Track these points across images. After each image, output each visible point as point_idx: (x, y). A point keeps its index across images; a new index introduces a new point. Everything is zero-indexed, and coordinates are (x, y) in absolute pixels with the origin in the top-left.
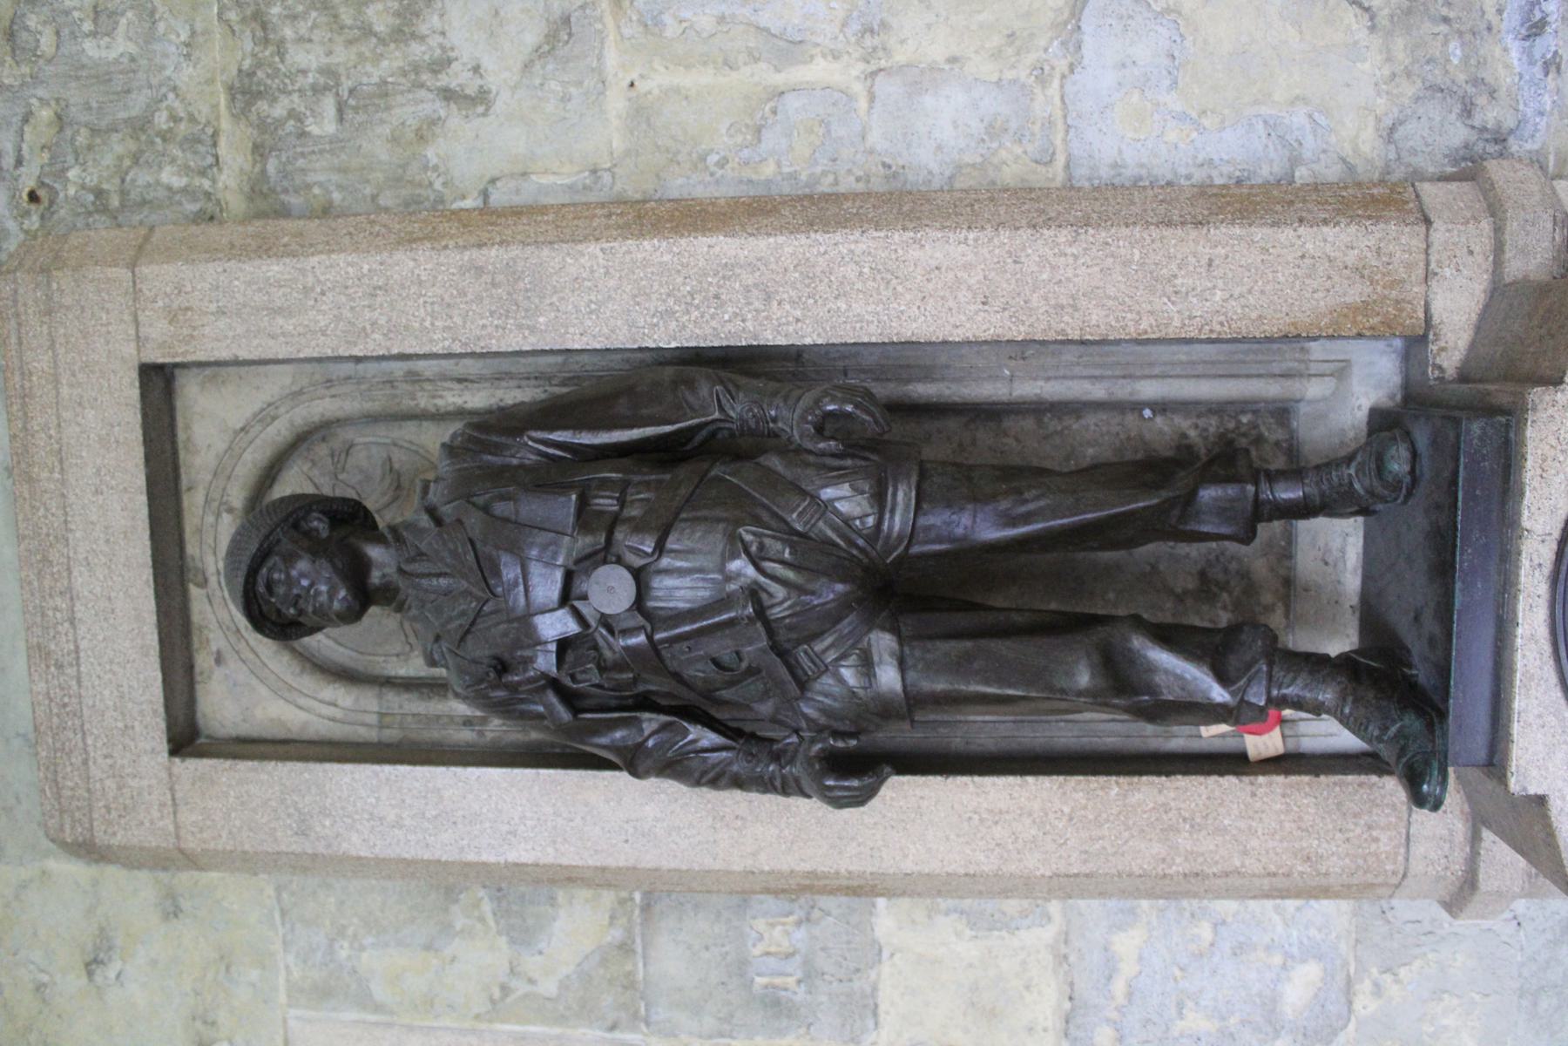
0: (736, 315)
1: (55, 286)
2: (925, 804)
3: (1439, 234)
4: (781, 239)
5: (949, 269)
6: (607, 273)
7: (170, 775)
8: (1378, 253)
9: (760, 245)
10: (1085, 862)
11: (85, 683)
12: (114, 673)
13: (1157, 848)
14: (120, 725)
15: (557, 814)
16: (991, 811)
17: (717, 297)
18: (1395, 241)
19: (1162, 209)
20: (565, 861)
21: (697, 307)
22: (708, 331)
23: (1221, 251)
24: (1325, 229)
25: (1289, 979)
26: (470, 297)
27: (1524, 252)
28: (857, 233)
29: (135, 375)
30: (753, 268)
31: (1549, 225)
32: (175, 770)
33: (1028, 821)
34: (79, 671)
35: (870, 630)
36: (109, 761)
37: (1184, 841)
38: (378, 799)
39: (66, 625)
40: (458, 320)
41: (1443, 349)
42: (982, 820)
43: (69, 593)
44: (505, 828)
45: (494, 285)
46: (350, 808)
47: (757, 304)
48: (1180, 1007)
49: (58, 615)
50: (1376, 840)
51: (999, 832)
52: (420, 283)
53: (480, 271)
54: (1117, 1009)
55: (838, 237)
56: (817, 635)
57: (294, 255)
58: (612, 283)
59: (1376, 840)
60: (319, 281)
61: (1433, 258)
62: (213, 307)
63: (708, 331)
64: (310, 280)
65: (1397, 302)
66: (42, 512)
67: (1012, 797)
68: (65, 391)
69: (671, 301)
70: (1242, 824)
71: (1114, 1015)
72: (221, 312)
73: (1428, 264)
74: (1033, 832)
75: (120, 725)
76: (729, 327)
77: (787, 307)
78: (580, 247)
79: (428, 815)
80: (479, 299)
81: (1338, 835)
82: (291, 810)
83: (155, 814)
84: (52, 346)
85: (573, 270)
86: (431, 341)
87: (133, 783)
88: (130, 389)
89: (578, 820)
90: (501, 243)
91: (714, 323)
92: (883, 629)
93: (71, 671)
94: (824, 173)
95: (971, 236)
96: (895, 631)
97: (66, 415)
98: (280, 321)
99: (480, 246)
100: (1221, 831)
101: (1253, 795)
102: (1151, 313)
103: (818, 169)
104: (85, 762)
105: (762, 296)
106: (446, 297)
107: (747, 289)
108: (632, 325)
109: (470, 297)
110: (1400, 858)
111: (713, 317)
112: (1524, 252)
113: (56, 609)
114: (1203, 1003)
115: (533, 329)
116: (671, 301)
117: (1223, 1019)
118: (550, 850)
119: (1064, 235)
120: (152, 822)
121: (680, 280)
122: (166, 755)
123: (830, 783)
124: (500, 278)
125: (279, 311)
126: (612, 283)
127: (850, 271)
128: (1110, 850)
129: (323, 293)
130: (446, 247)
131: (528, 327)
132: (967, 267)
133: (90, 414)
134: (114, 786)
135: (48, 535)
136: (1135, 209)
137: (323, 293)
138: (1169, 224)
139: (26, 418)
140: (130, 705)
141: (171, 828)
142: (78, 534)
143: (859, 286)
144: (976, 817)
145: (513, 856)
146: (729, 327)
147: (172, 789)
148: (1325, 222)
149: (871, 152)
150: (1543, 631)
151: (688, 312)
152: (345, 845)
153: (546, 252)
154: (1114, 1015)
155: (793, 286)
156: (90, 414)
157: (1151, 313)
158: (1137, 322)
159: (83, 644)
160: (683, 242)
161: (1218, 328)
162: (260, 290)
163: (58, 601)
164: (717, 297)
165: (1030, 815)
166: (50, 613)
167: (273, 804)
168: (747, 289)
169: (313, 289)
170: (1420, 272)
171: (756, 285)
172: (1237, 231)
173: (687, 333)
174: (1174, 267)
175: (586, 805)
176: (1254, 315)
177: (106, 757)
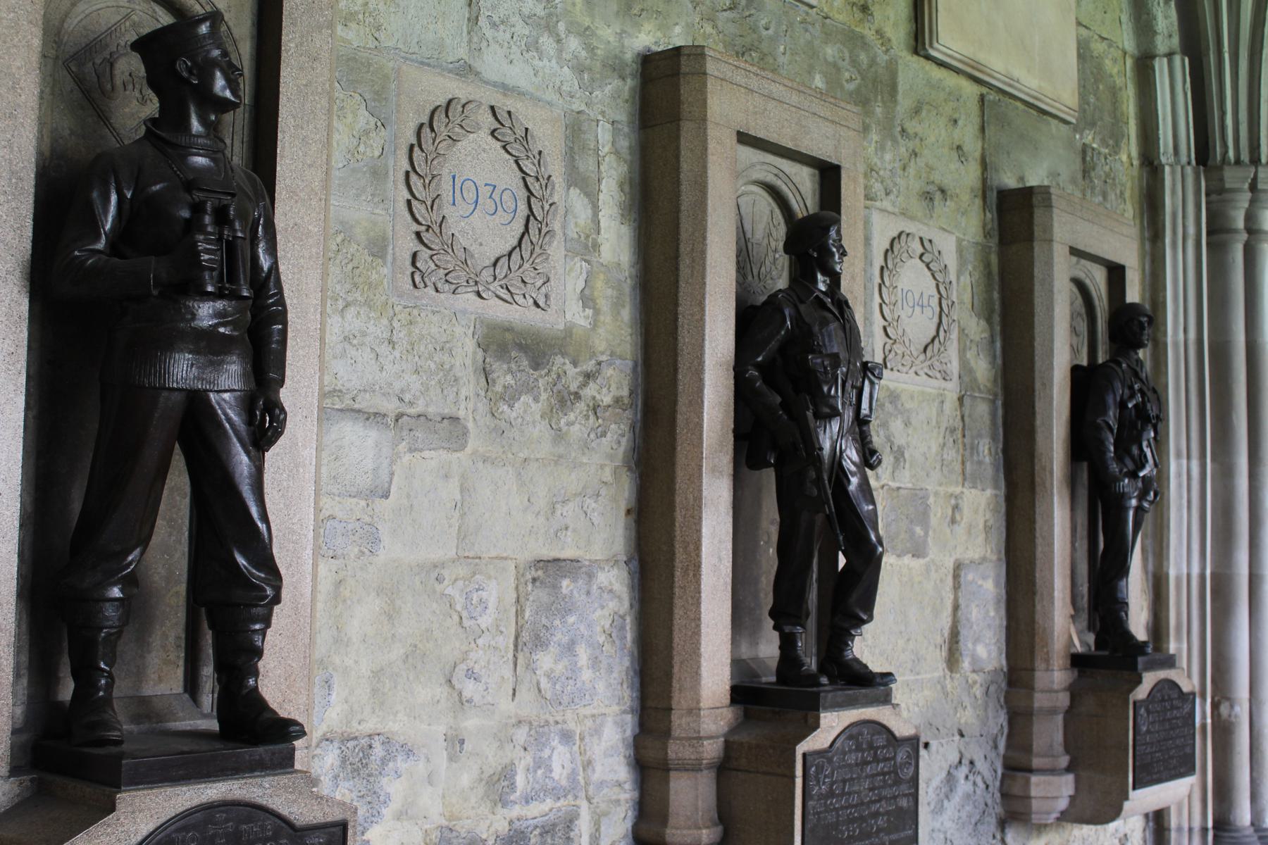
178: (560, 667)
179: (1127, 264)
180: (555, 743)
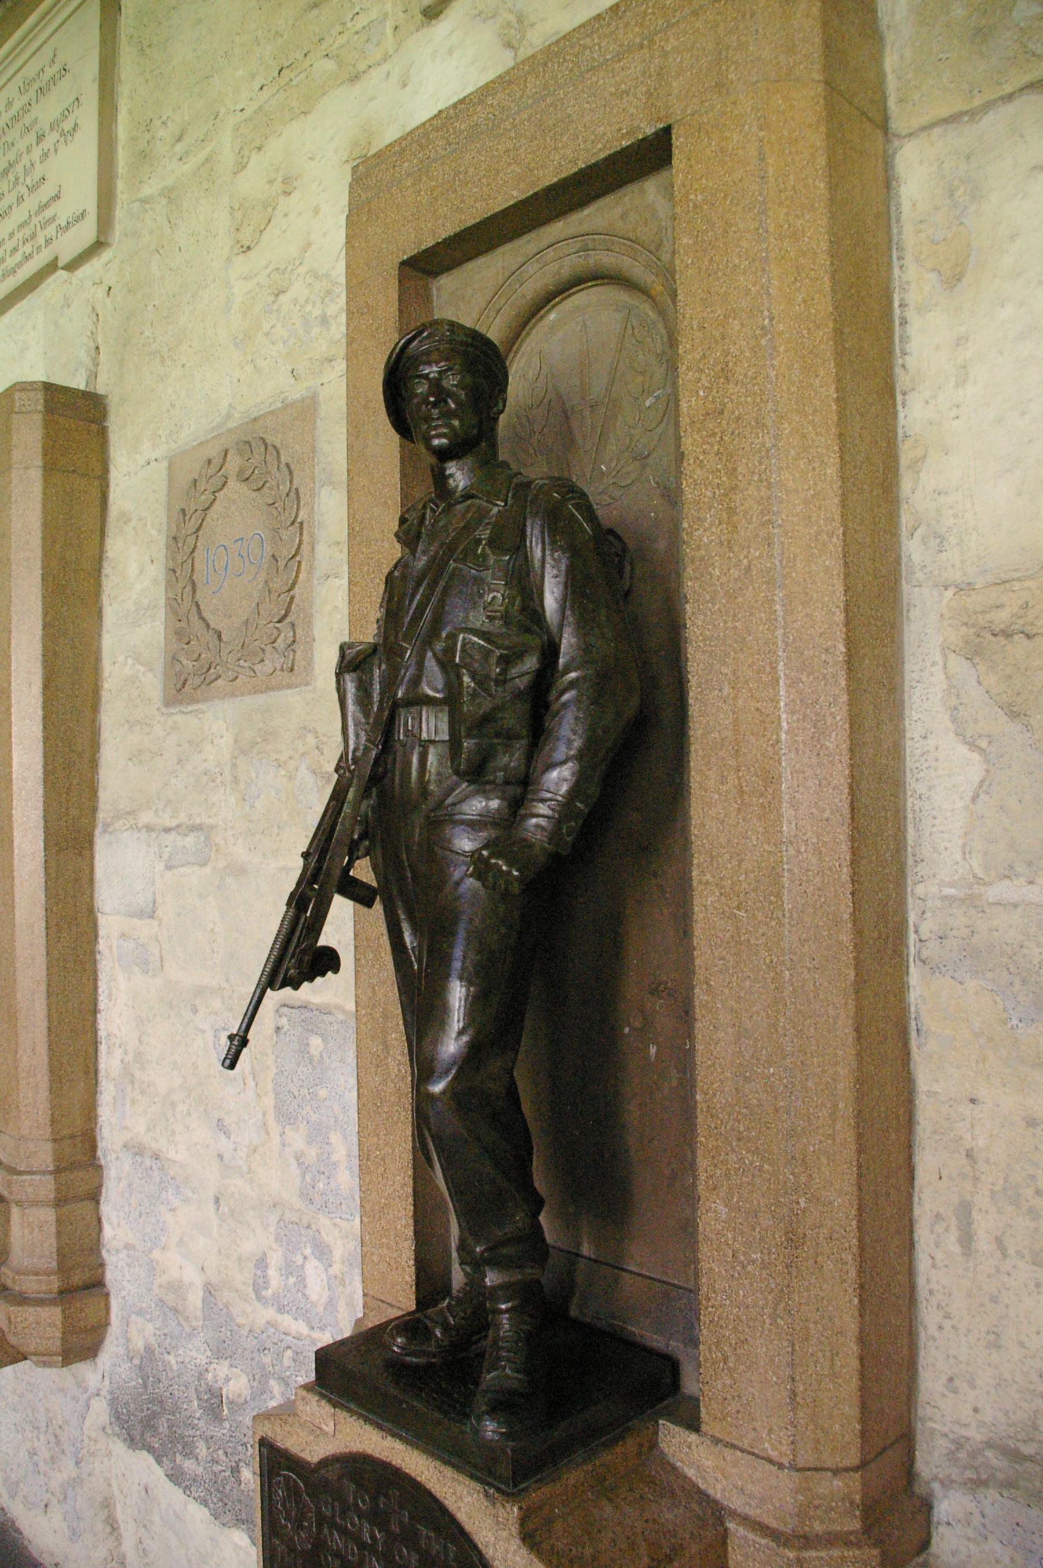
178: (312, 1152)
180: (308, 1251)
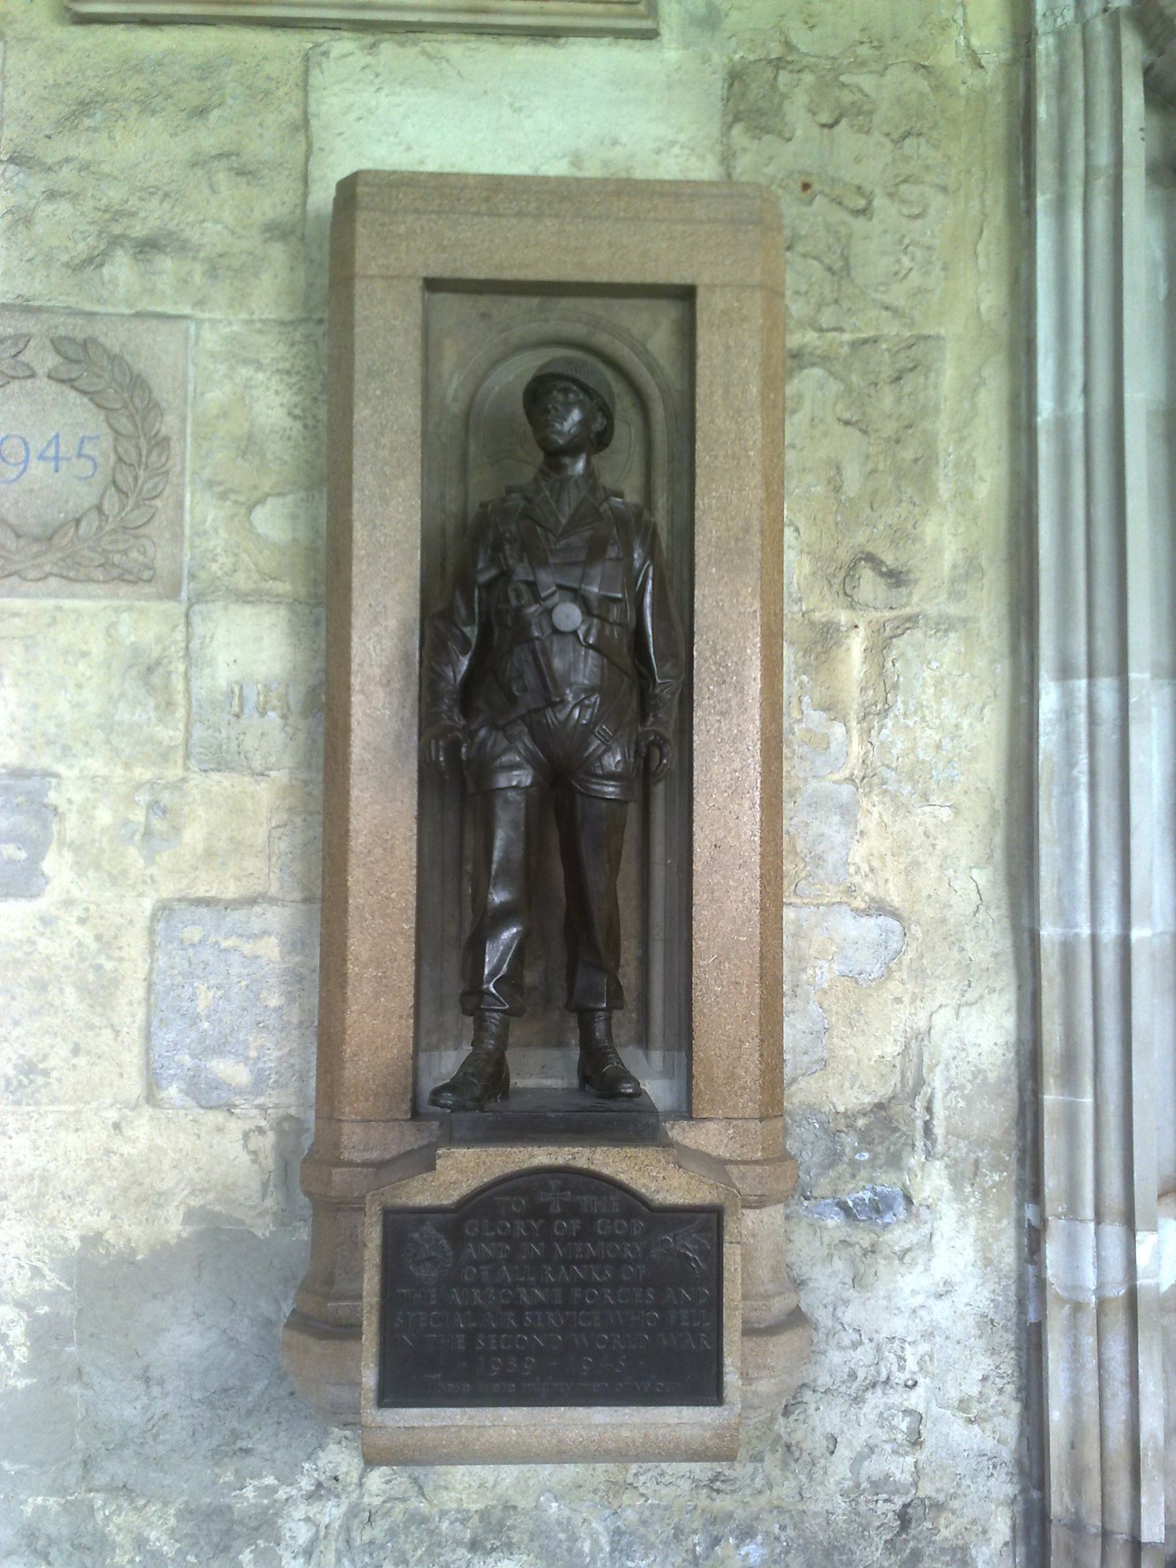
0: (712, 693)
1: (750, 227)
2: (399, 804)
3: (755, 1125)
4: (758, 723)
5: (737, 825)
6: (740, 613)
7: (410, 277)
8: (741, 1088)
9: (756, 712)
10: (357, 908)
11: (476, 220)
12: (483, 242)
13: (365, 956)
14: (445, 242)
15: (389, 560)
16: (392, 846)
17: (724, 682)
18: (748, 1105)
19: (770, 956)
20: (355, 562)
21: (718, 670)
22: (703, 676)
23: (745, 990)
24: (757, 1055)
25: (237, 1063)
26: (731, 524)
27: (743, 1177)
28: (759, 769)
29: (689, 281)
30: (741, 704)
31: (759, 1192)
32: (413, 282)
33: (386, 871)
34: (483, 215)
35: (533, 768)
36: (419, 230)
37: (371, 972)
38: (396, 432)
39: (517, 209)
40: (716, 514)
41: (684, 1130)
42: (386, 840)
43: (539, 216)
44: (378, 522)
45: (737, 540)
46: (389, 411)
47: (718, 707)
48: (219, 987)
49: (523, 203)
50: (367, 1100)
51: (378, 851)
52: (740, 490)
53: (746, 530)
54: (217, 942)
55: (758, 758)
56: (534, 739)
57: (763, 403)
58: (735, 616)
59: (367, 1100)
60: (745, 420)
61: (740, 1123)
62: (731, 343)
63: (703, 676)
64: (745, 414)
65: (712, 1100)
66: (597, 199)
67: (402, 860)
68: (680, 228)
69: (722, 653)
70: (381, 1010)
71: (212, 939)
72: (728, 348)
73: (736, 1119)
74: (379, 874)
75: (445, 242)
76: (705, 689)
77: (716, 725)
78: (758, 597)
79: (386, 468)
80: (728, 529)
81: (371, 1074)
82: (386, 367)
83: (381, 261)
84: (709, 221)
85: (743, 592)
86: (703, 496)
87: (403, 247)
88: (678, 277)
89: (384, 573)
90: (762, 545)
91: (708, 680)
92: (534, 777)
93: (484, 208)
94: (793, 751)
95: (757, 839)
96: (532, 785)
97: (663, 227)
98: (720, 391)
99: (762, 532)
100: (377, 996)
101: (401, 1017)
102: (708, 947)
103: (796, 747)
104: (416, 211)
105: (724, 710)
106: (731, 508)
107: (728, 701)
108: (709, 628)
109: (731, 524)
110: (354, 1117)
111: (712, 679)
112: (743, 1177)
113: (528, 202)
114: (221, 1003)
115: (708, 564)
116: (722, 653)
117: (208, 1017)
118: (363, 552)
119: (756, 895)
120: (374, 258)
121: (735, 659)
122: (424, 274)
123: (441, 743)
124: (741, 544)
125: (727, 391)
126: (735, 616)
127: (737, 764)
128: (365, 924)
129: (737, 423)
130: (762, 508)
131: (709, 561)
132: (739, 836)
133: (664, 245)
134: (400, 232)
135: (580, 202)
136: (770, 939)
137: (737, 423)
138: (762, 959)
139: (662, 195)
140: (460, 252)
141: (370, 272)
142: (581, 226)
143: (728, 770)
144: (389, 837)
145: (357, 525)
146: (705, 689)
147: (398, 277)
148: (761, 1055)
149: (806, 780)
150: (510, 1168)
151: (715, 663)
152: (362, 404)
153: (756, 575)
154: (212, 939)
155: (730, 729)
156: (664, 245)
157: (708, 947)
158: (702, 939)
159: (504, 221)
160: (759, 662)
161: (699, 988)
162: (741, 378)
163: (533, 205)
164: (724, 682)
165: (390, 871)
166: (525, 197)
167: (391, 353)
168: (728, 701)
169: (740, 415)
170: (731, 1115)
171: (730, 706)
172: (757, 1000)
173: (702, 662)
174: (735, 961)
175: (396, 580)
176: (706, 1010)
177: (422, 228)
179: (703, 280)
